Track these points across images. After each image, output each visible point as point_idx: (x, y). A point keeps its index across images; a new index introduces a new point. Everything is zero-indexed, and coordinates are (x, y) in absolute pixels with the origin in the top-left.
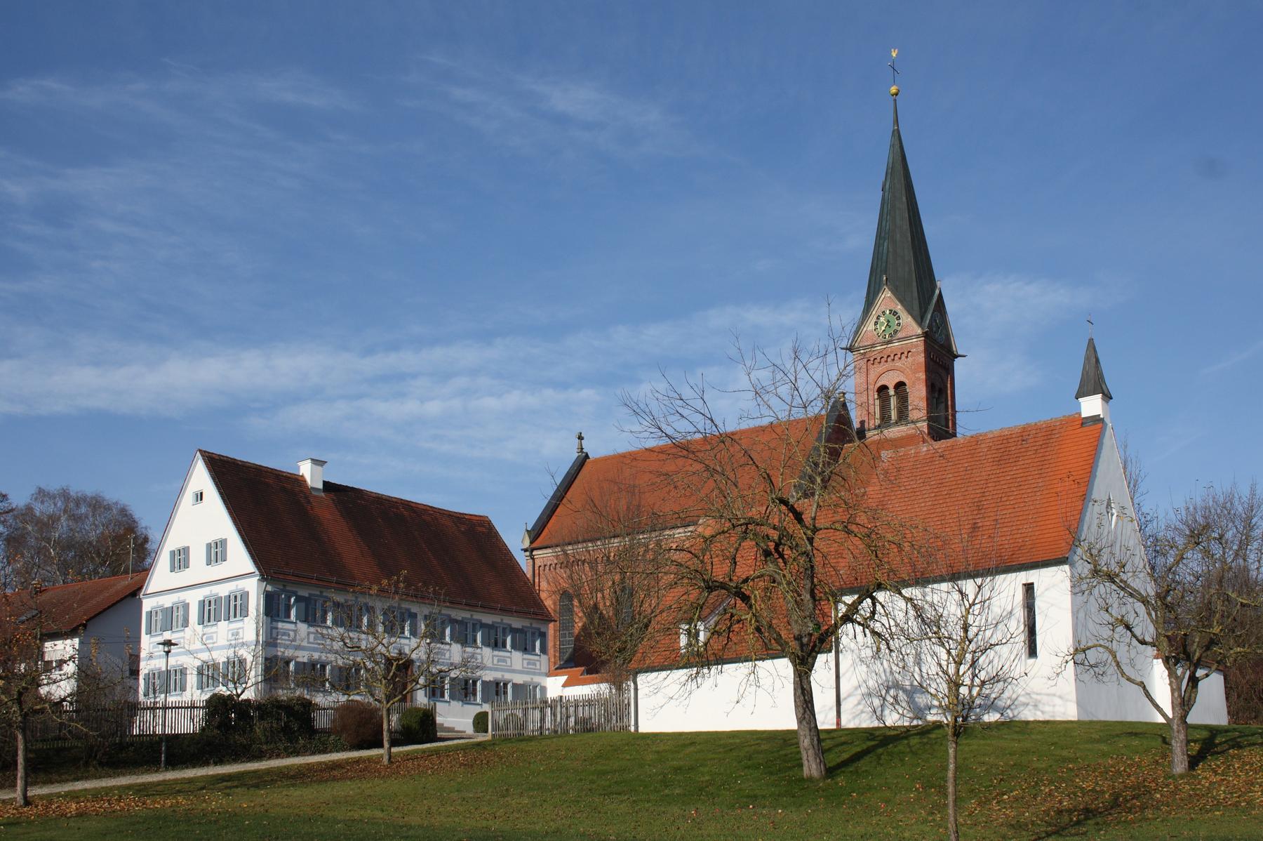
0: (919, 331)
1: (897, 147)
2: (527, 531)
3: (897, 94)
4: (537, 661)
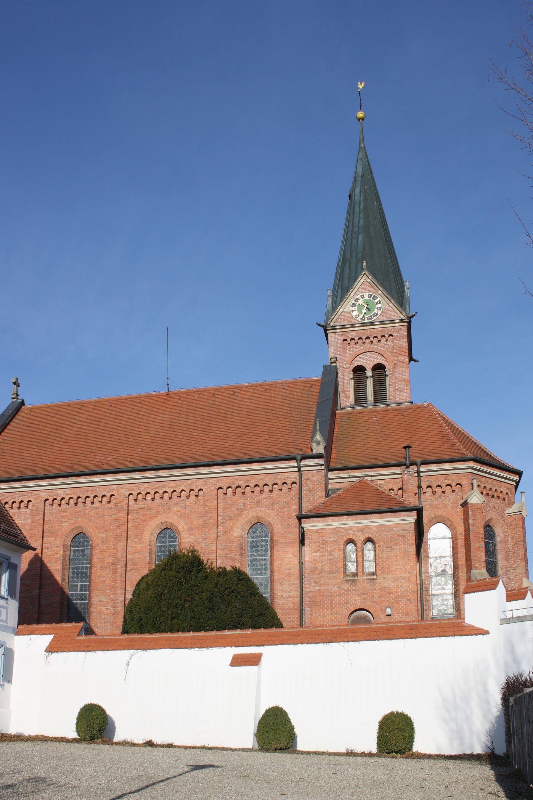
3: (363, 119)
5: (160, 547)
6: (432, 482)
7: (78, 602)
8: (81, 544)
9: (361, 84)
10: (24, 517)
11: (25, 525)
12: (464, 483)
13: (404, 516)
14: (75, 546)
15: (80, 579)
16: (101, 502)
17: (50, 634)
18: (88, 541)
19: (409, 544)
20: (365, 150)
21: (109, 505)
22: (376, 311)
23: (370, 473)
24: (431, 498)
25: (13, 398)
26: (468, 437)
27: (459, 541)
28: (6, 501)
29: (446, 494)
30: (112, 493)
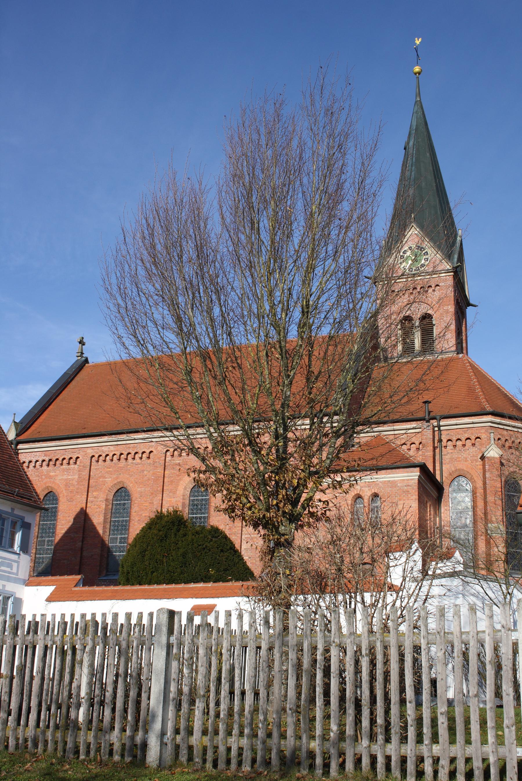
0: (448, 266)
1: (420, 114)
2: (15, 422)
3: (419, 73)
4: (15, 561)
5: (193, 501)
6: (452, 436)
7: (117, 554)
8: (123, 498)
9: (418, 40)
10: (73, 472)
11: (73, 480)
12: (483, 436)
13: (408, 472)
14: (117, 500)
15: (120, 532)
16: (141, 458)
17: (53, 585)
18: (129, 496)
19: (413, 499)
20: (421, 103)
21: (149, 461)
22: (423, 262)
23: (392, 427)
24: (451, 451)
25: (78, 357)
26: (499, 389)
27: (478, 494)
28: (57, 458)
29: (467, 447)
30: (151, 450)
